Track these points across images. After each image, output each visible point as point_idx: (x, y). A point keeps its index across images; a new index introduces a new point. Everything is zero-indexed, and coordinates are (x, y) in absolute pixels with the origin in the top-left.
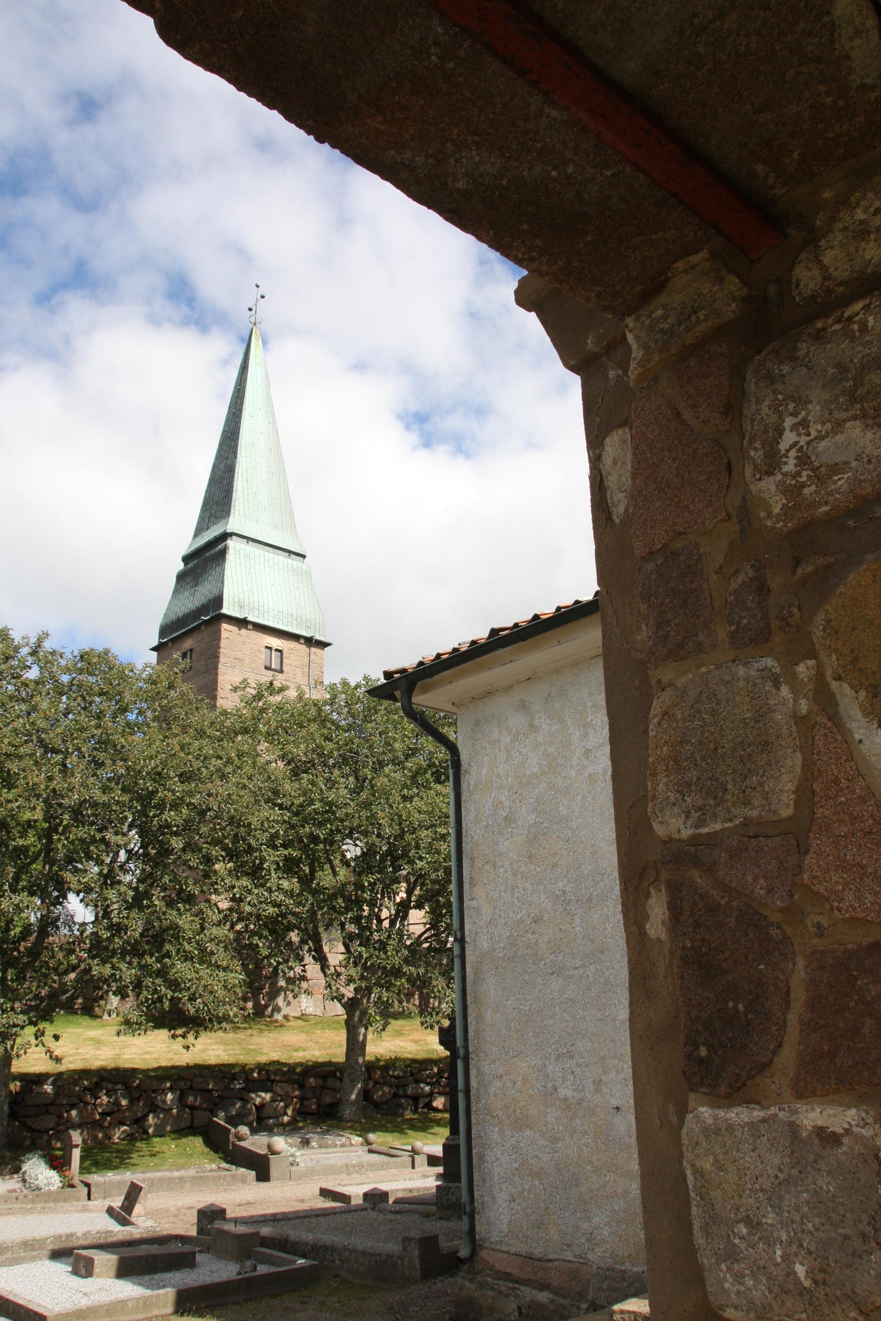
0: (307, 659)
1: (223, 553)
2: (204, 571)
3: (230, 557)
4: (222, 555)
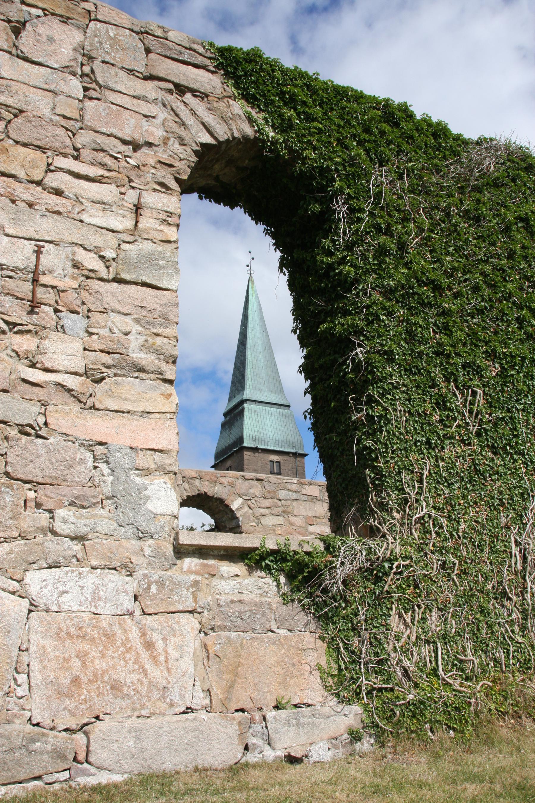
0: (294, 465)
1: (243, 411)
3: (246, 413)
4: (241, 413)
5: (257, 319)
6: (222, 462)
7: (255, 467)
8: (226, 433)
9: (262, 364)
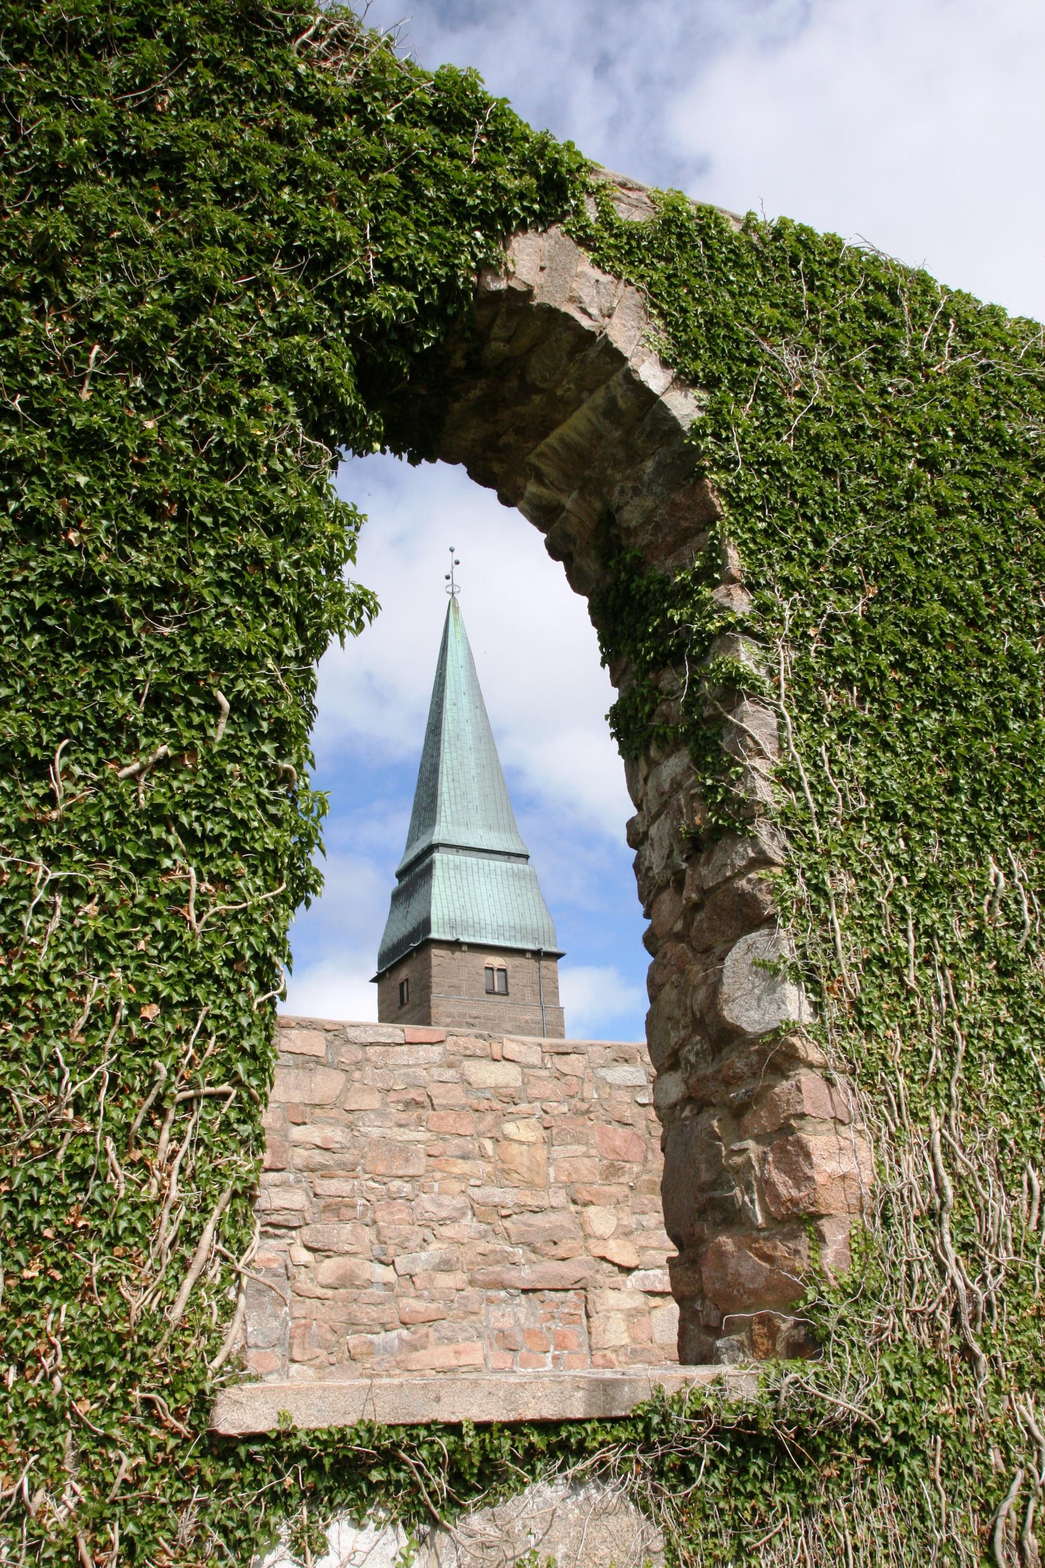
0: (536, 977)
1: (430, 868)
2: (415, 890)
3: (438, 872)
4: (429, 869)
5: (463, 681)
6: (391, 970)
7: (455, 981)
8: (401, 911)
9: (473, 772)
